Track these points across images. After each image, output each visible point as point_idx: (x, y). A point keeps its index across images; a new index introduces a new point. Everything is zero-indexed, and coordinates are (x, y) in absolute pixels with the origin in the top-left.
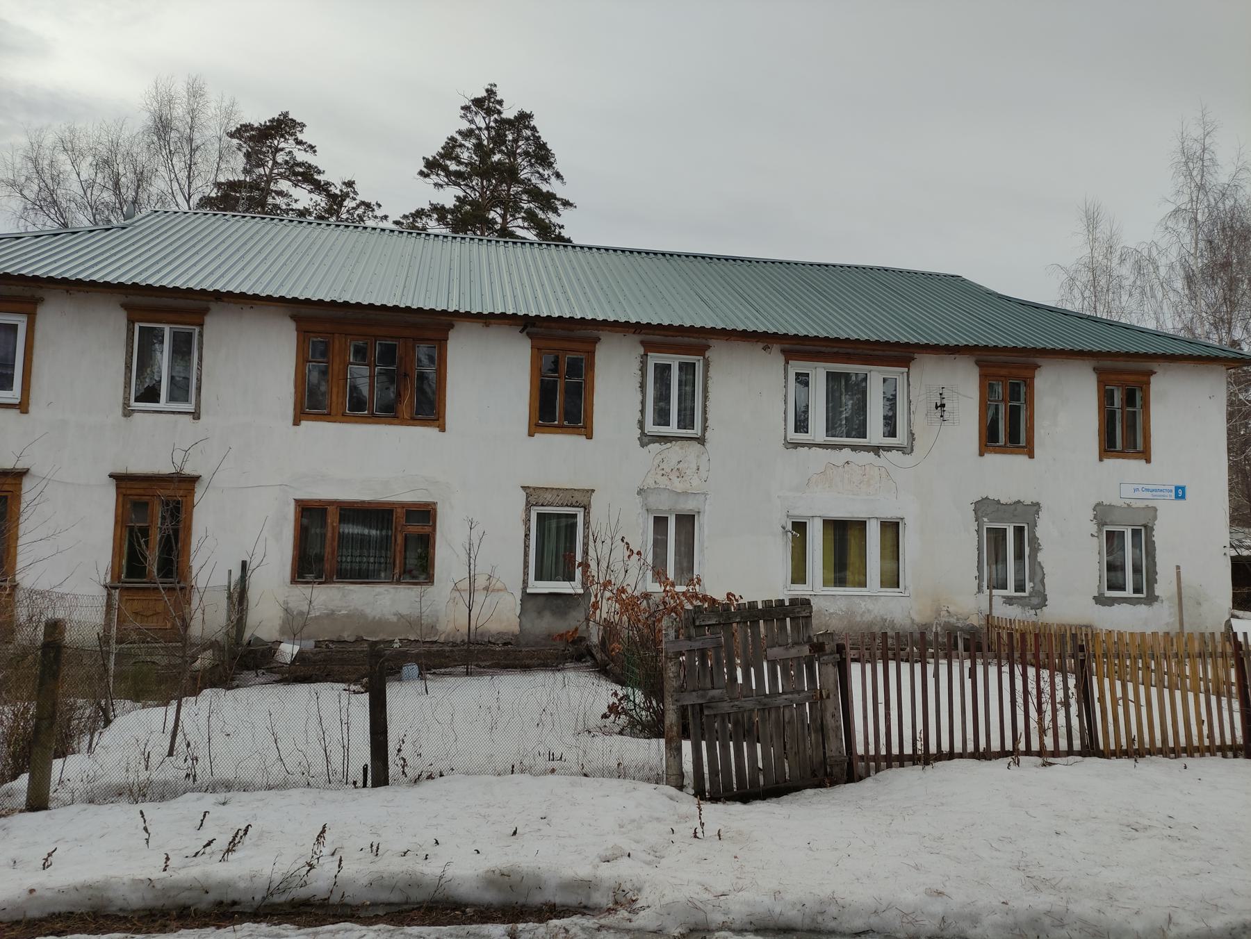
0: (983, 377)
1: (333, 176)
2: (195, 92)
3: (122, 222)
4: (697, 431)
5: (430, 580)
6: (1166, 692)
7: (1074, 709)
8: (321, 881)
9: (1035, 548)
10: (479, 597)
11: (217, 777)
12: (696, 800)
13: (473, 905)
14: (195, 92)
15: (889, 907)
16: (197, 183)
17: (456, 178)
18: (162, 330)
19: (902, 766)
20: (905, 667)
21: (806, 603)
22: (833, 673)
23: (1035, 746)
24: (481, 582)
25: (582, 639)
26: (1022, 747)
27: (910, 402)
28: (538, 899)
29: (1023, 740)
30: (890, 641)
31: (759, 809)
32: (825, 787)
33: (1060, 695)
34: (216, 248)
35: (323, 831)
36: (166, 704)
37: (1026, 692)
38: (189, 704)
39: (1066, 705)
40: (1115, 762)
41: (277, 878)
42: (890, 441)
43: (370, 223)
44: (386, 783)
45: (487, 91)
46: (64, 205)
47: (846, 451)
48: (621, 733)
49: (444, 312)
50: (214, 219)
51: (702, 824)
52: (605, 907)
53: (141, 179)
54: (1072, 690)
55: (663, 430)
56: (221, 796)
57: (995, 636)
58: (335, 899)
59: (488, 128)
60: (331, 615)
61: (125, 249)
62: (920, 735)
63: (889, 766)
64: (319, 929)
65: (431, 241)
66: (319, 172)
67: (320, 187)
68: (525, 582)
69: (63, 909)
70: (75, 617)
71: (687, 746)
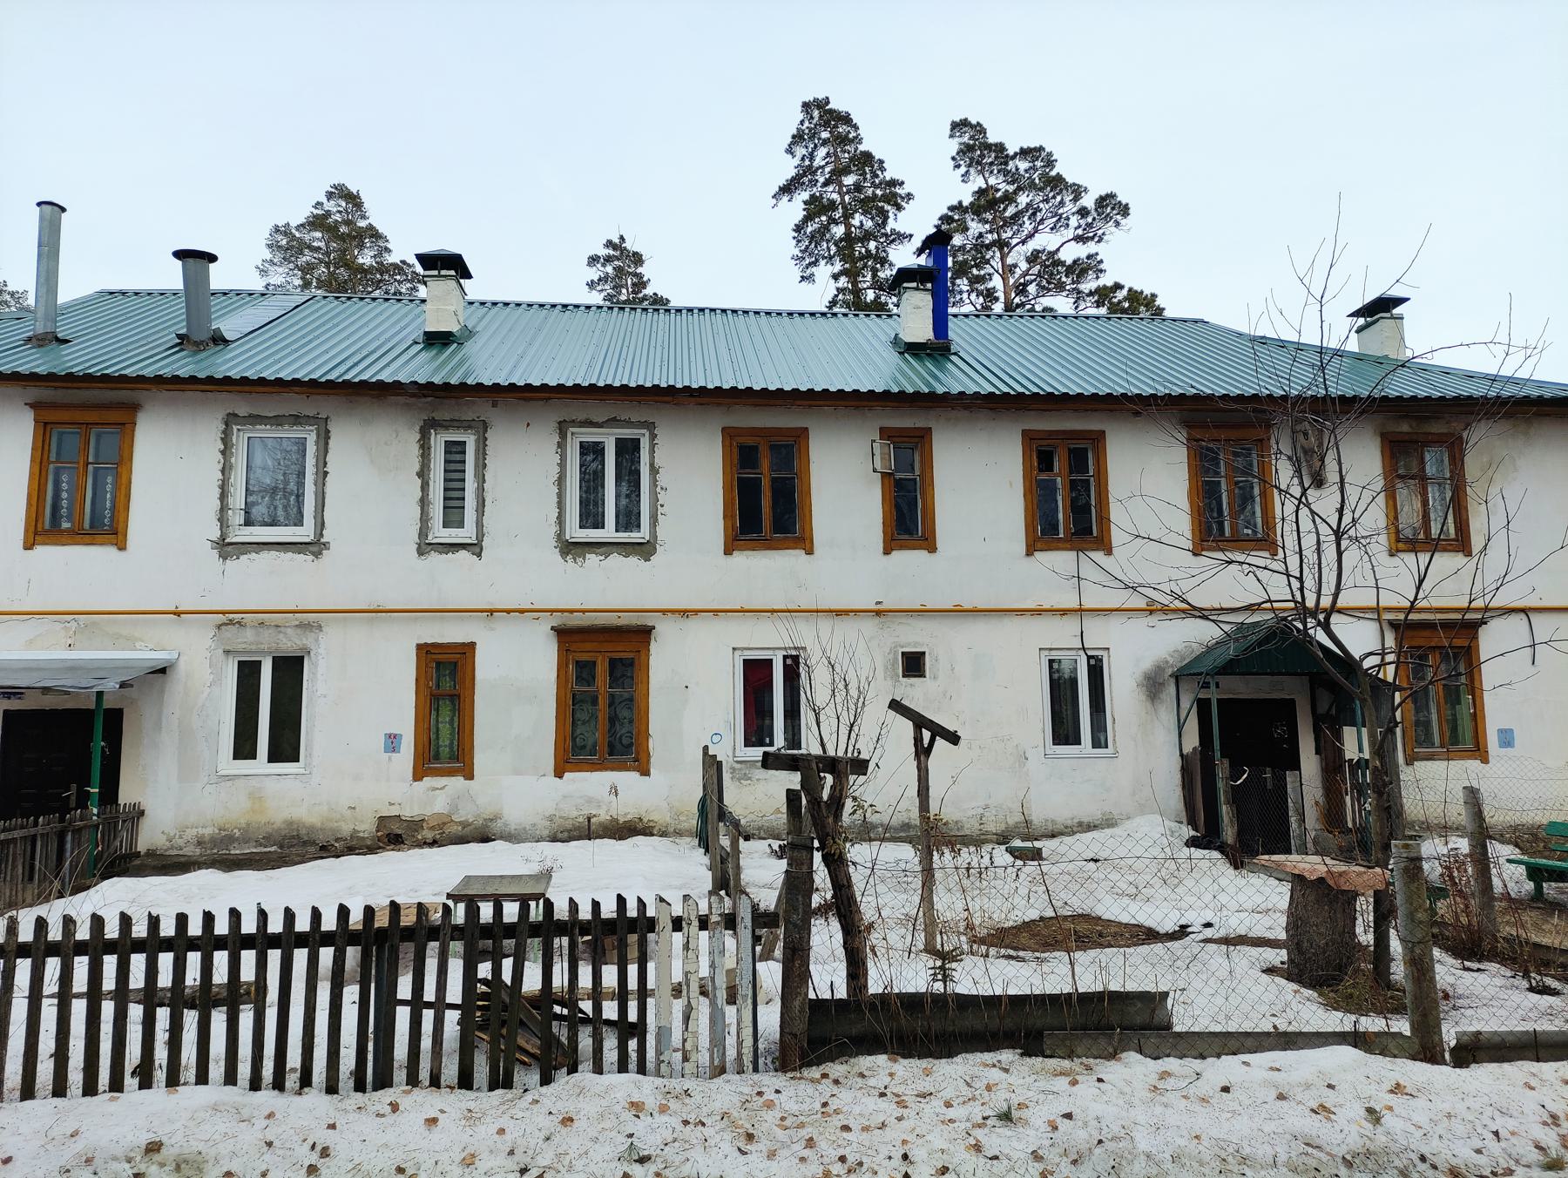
0: (1193, 445)
34: (689, 349)
61: (1090, 358)
65: (696, 315)
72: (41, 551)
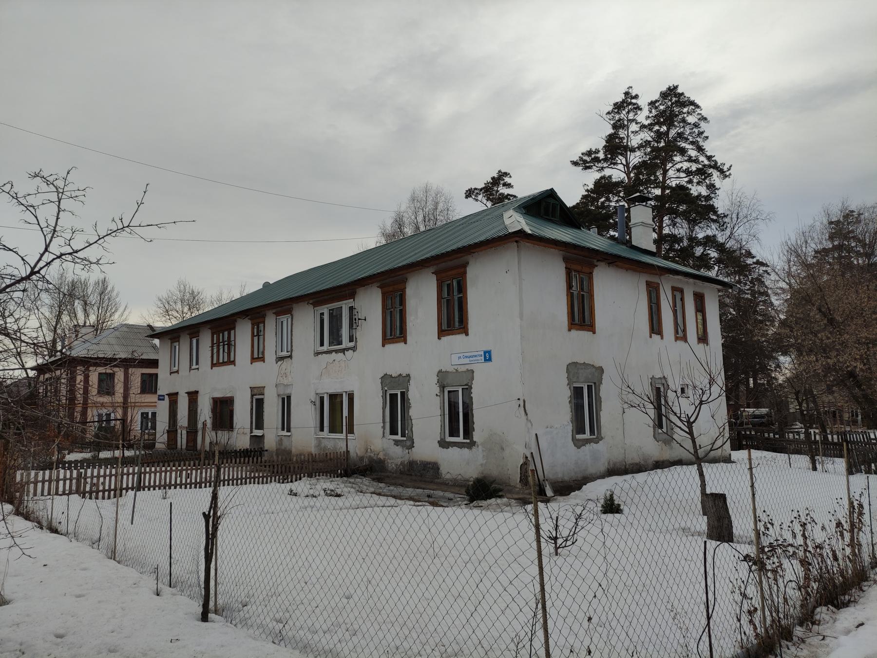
0: (383, 294)
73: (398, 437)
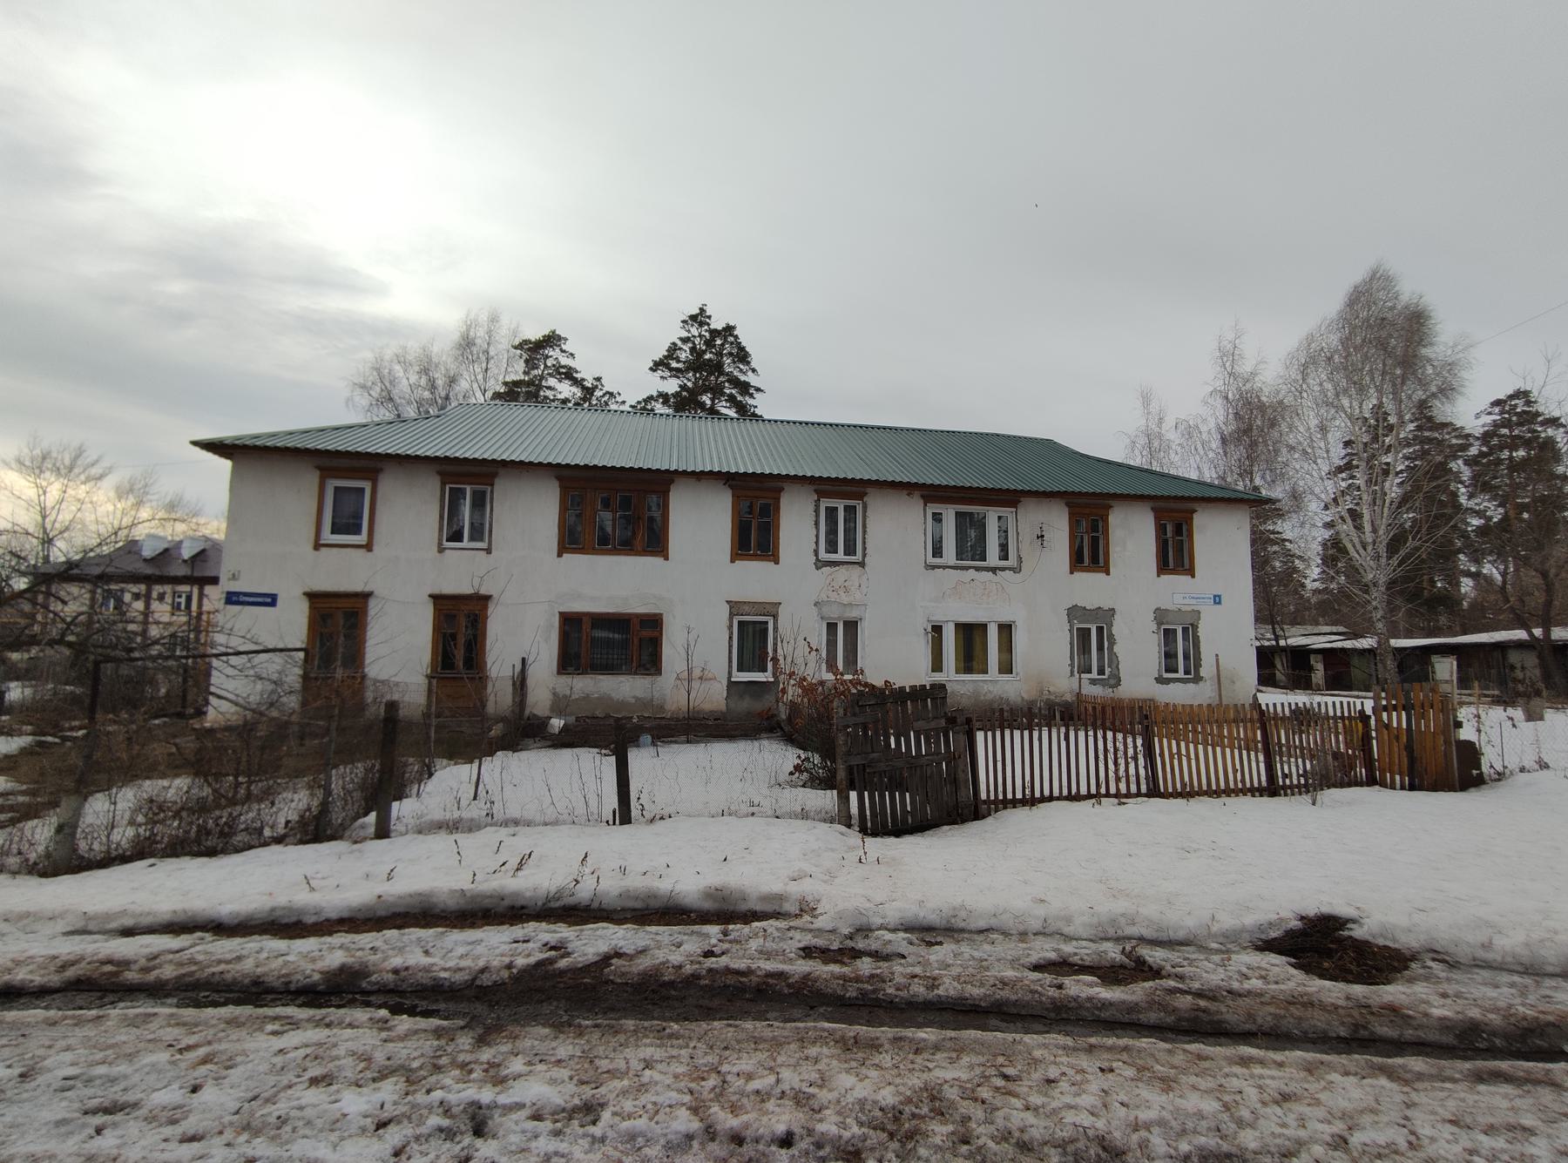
0: (1071, 515)
1: (587, 374)
2: (494, 319)
3: (437, 413)
4: (858, 557)
5: (659, 672)
6: (1210, 748)
7: (1141, 761)
8: (584, 892)
9: (1112, 642)
10: (695, 684)
11: (508, 816)
12: (861, 835)
13: (695, 911)
14: (494, 319)
15: (1005, 911)
16: (492, 382)
17: (677, 372)
18: (465, 489)
19: (1015, 807)
20: (1017, 733)
21: (942, 687)
22: (963, 738)
23: (1113, 790)
24: (697, 673)
25: (773, 716)
26: (1103, 791)
27: (1018, 534)
28: (743, 907)
29: (1104, 786)
30: (1005, 714)
31: (908, 841)
32: (957, 824)
33: (1131, 752)
35: (586, 857)
36: (471, 762)
37: (1106, 750)
38: (487, 761)
39: (1135, 758)
40: (1172, 801)
41: (553, 889)
42: (1003, 563)
43: (613, 407)
44: (629, 822)
45: (700, 309)
46: (398, 401)
47: (972, 571)
48: (803, 786)
49: (667, 471)
50: (501, 408)
51: (865, 853)
52: (793, 914)
53: (452, 381)
54: (1140, 748)
55: (833, 557)
56: (511, 830)
57: (1083, 709)
58: (595, 905)
59: (700, 336)
60: (587, 698)
62: (1028, 784)
63: (1005, 808)
64: (584, 927)
66: (577, 372)
67: (577, 382)
68: (730, 673)
69: (401, 910)
70: (406, 698)
71: (853, 795)
72: (1077, 575)
73: (1094, 675)
